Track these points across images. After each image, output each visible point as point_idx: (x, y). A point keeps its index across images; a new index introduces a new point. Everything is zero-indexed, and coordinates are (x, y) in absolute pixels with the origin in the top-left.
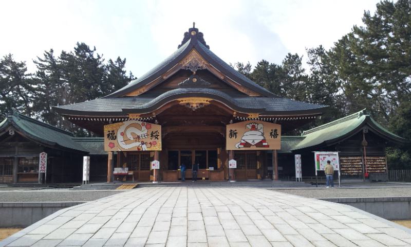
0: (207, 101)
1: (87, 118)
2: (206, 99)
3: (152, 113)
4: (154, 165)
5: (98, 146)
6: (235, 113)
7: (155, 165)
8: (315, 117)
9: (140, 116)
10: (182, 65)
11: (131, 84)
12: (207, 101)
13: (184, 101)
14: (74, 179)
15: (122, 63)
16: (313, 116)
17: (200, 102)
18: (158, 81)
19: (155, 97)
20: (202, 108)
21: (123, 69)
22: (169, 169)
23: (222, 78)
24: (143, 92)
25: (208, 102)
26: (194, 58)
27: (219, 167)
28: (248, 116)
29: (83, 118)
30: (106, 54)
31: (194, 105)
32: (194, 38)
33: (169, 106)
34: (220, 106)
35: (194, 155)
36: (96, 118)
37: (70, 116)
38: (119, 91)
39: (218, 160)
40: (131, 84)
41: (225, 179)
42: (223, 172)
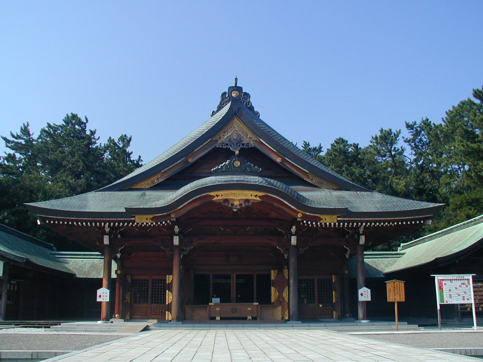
0: (256, 196)
1: (73, 221)
2: (254, 193)
3: (170, 215)
4: (362, 295)
5: (88, 265)
6: (299, 215)
7: (103, 295)
8: (422, 222)
9: (152, 219)
10: (217, 141)
11: (137, 172)
12: (256, 196)
13: (220, 196)
14: (299, 283)
15: (126, 140)
16: (420, 220)
17: (246, 198)
18: (179, 169)
19: (178, 188)
20: (247, 207)
21: (129, 150)
22: (194, 304)
23: (279, 160)
24: (156, 182)
25: (258, 199)
26: (237, 130)
27: (273, 300)
28: (321, 219)
29: (68, 221)
30: (104, 131)
31: (236, 203)
32: (238, 103)
33: (197, 204)
34: (276, 204)
35: (233, 282)
36: (86, 222)
37: (48, 219)
38: (121, 180)
39: (273, 289)
40: (137, 172)
41: (283, 318)
42: (280, 308)
